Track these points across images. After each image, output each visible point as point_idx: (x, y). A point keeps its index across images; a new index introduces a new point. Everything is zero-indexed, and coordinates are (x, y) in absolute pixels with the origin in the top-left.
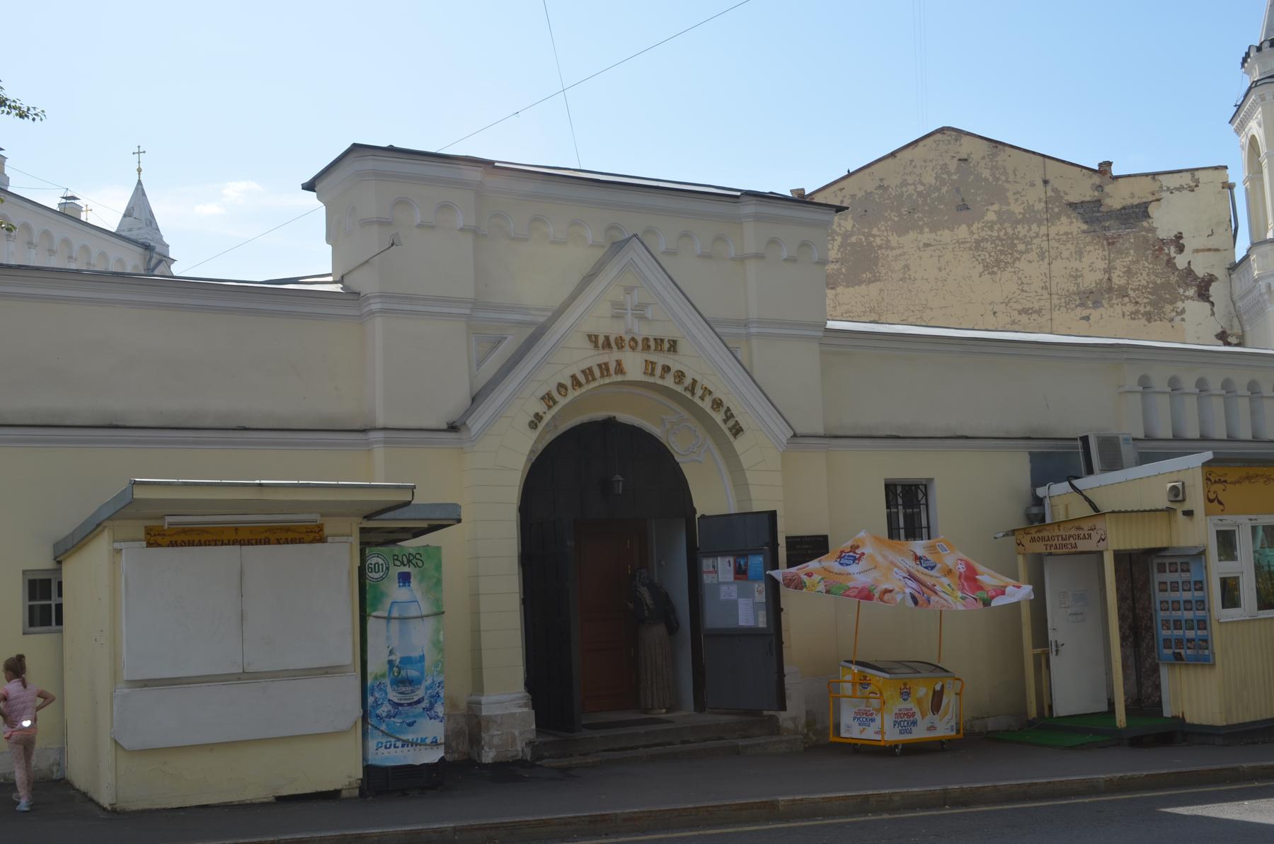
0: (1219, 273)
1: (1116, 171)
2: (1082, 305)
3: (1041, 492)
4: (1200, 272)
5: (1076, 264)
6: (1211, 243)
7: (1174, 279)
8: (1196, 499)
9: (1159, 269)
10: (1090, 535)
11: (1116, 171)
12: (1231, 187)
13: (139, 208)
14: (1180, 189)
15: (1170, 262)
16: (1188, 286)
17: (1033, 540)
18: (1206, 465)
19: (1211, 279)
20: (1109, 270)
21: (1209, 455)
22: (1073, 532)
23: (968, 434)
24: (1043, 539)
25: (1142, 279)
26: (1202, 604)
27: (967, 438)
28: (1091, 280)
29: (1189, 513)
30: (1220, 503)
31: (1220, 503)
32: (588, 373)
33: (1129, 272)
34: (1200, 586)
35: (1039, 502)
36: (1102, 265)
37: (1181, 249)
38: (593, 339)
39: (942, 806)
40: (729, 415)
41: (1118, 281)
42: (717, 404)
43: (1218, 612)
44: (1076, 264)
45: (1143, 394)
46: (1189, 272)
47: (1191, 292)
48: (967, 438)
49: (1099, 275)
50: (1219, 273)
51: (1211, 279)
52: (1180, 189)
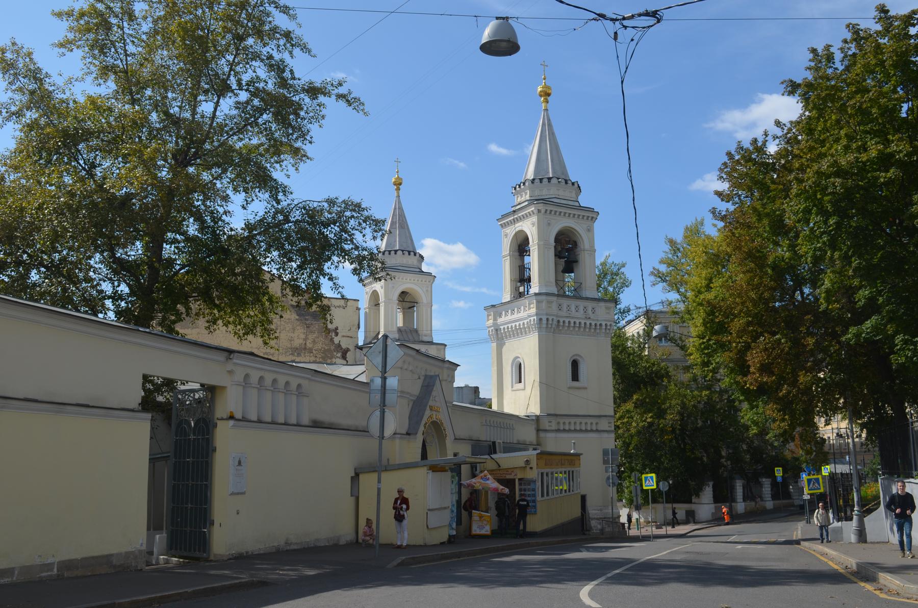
0: (352, 348)
2: (292, 354)
4: (344, 346)
5: (292, 335)
6: (349, 334)
7: (333, 348)
8: (534, 463)
9: (327, 342)
12: (358, 309)
13: (792, 88)
14: (339, 307)
15: (332, 340)
16: (338, 352)
19: (348, 350)
20: (305, 339)
23: (39, 398)
25: (319, 346)
26: (534, 495)
27: (87, 406)
28: (297, 343)
29: (531, 468)
33: (314, 342)
34: (534, 490)
36: (303, 336)
37: (337, 334)
39: (194, 592)
41: (309, 345)
43: (539, 498)
44: (292, 335)
45: (244, 387)
46: (339, 345)
47: (339, 355)
48: (87, 406)
49: (301, 341)
50: (352, 348)
51: (348, 350)
52: (339, 307)
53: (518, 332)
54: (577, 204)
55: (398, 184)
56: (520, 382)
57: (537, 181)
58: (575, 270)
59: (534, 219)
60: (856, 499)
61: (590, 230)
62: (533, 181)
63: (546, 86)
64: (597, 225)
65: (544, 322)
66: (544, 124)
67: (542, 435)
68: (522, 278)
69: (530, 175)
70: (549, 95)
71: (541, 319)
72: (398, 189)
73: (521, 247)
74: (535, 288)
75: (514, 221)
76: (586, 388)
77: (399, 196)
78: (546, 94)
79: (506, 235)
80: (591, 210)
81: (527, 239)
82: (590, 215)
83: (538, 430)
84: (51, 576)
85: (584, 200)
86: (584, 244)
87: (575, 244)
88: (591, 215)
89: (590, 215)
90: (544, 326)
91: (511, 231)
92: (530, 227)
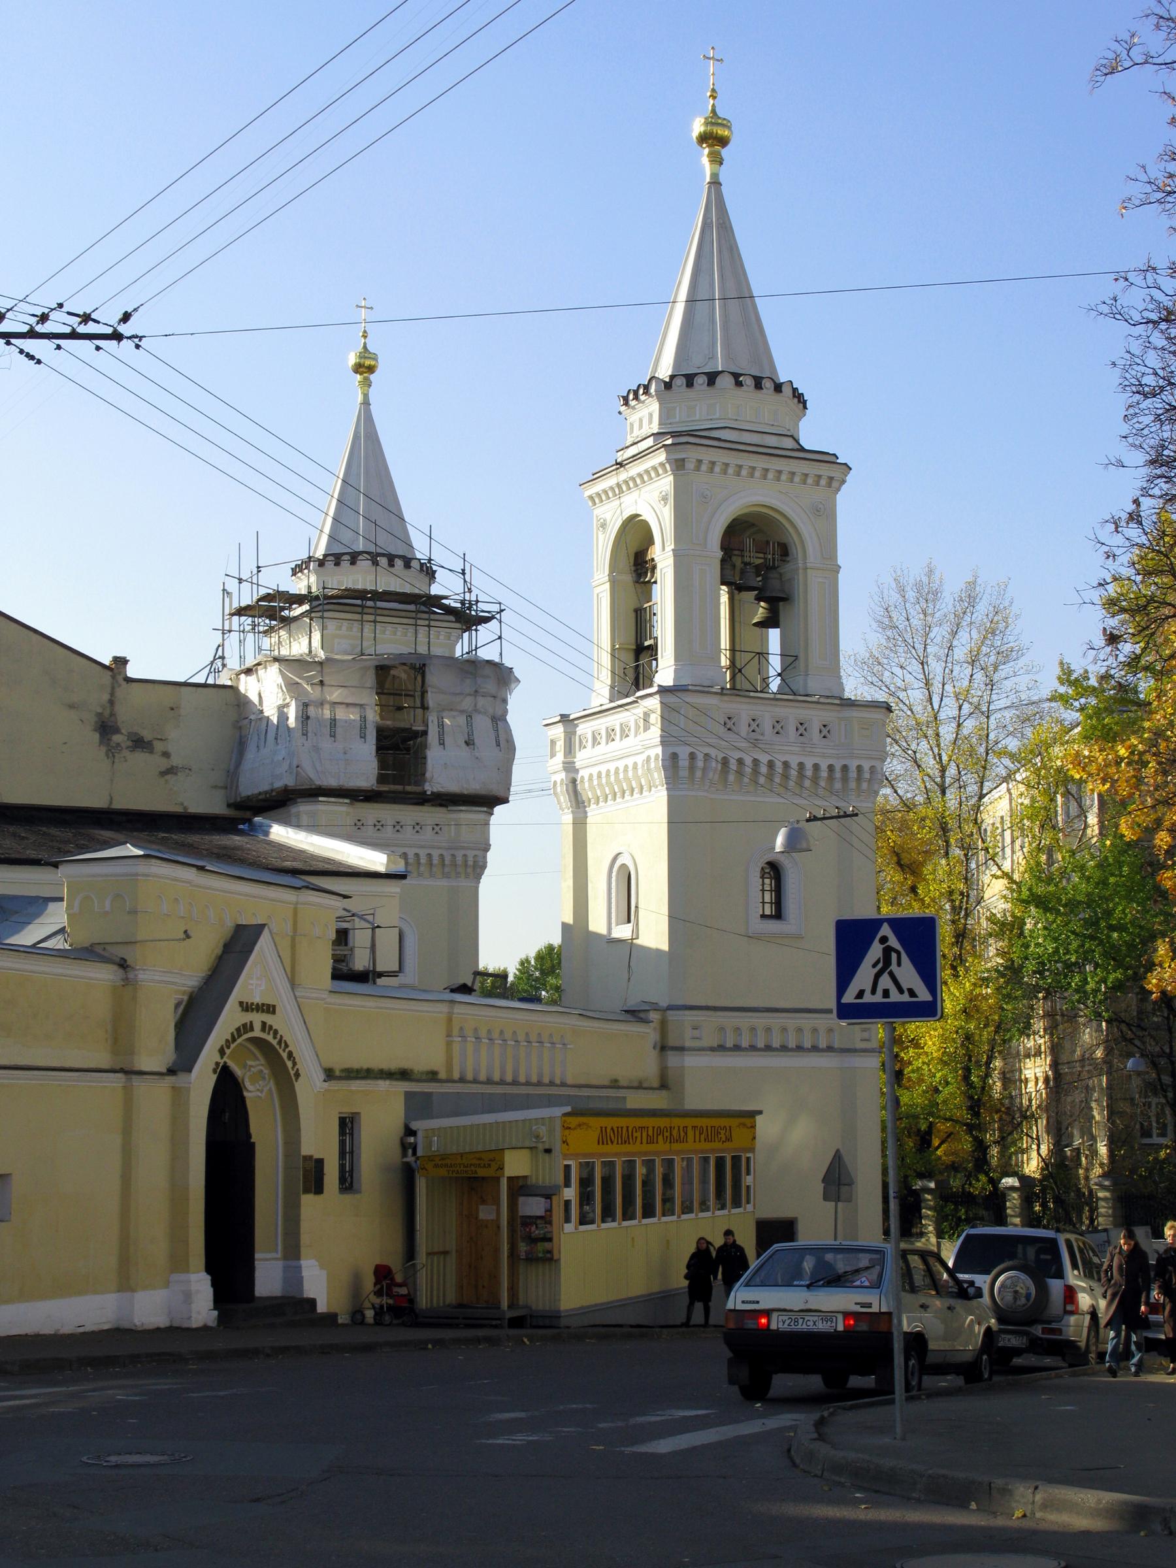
1: (132, 671)
3: (414, 1125)
10: (489, 1165)
11: (132, 671)
17: (436, 1166)
21: (568, 1109)
22: (475, 1161)
24: (446, 1165)
32: (238, 1030)
35: (410, 1132)
38: (241, 1003)
40: (295, 1064)
42: (290, 1055)
53: (622, 788)
54: (789, 443)
55: (365, 368)
56: (629, 921)
57: (680, 381)
58: (781, 623)
59: (666, 483)
60: (898, 1419)
61: (826, 515)
62: (668, 385)
63: (714, 118)
64: (847, 501)
65: (684, 762)
66: (706, 225)
67: (673, 1060)
68: (635, 658)
69: (665, 371)
70: (723, 142)
71: (674, 756)
72: (367, 383)
73: (635, 562)
74: (665, 673)
75: (618, 490)
76: (799, 937)
77: (366, 403)
78: (714, 140)
79: (603, 526)
81: (645, 527)
82: (829, 469)
83: (663, 1048)
84: (1003, 1529)
85: (811, 434)
87: (784, 551)
88: (825, 471)
89: (829, 469)
90: (684, 773)
91: (613, 514)
92: (653, 500)
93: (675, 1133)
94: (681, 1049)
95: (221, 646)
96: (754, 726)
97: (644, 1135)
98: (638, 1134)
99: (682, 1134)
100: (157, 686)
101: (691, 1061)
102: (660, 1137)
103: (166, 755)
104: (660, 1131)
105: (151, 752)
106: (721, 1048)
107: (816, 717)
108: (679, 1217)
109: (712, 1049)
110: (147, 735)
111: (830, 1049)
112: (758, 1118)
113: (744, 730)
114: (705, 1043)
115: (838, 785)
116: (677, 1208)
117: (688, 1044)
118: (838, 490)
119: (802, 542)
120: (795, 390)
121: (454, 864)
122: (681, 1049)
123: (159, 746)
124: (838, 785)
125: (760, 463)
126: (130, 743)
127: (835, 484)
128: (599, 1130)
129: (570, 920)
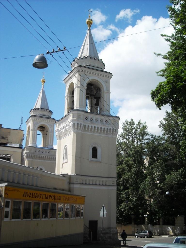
1: (3, 126)
18: (6, 186)
30: (7, 195)
31: (7, 195)
61: (108, 83)
68: (71, 107)
73: (72, 92)
80: (109, 73)
82: (109, 75)
86: (104, 88)
88: (109, 75)
92: (75, 80)
93: (56, 197)
94: (73, 183)
95: (21, 125)
96: (92, 119)
97: (44, 197)
98: (42, 196)
99: (59, 198)
100: (7, 129)
101: (76, 186)
102: (50, 198)
103: (7, 140)
104: (51, 196)
105: (5, 139)
106: (82, 184)
107: (104, 119)
108: (41, 219)
109: (80, 184)
110: (4, 136)
111: (106, 185)
112: (85, 197)
113: (89, 120)
114: (78, 182)
115: (109, 132)
116: (22, 215)
117: (75, 182)
118: (110, 79)
119: (103, 87)
120: (102, 62)
121: (52, 158)
122: (73, 183)
123: (6, 139)
124: (109, 132)
125: (95, 71)
126: (1, 138)
127: (110, 77)
128: (24, 193)
129: (3, 126)
